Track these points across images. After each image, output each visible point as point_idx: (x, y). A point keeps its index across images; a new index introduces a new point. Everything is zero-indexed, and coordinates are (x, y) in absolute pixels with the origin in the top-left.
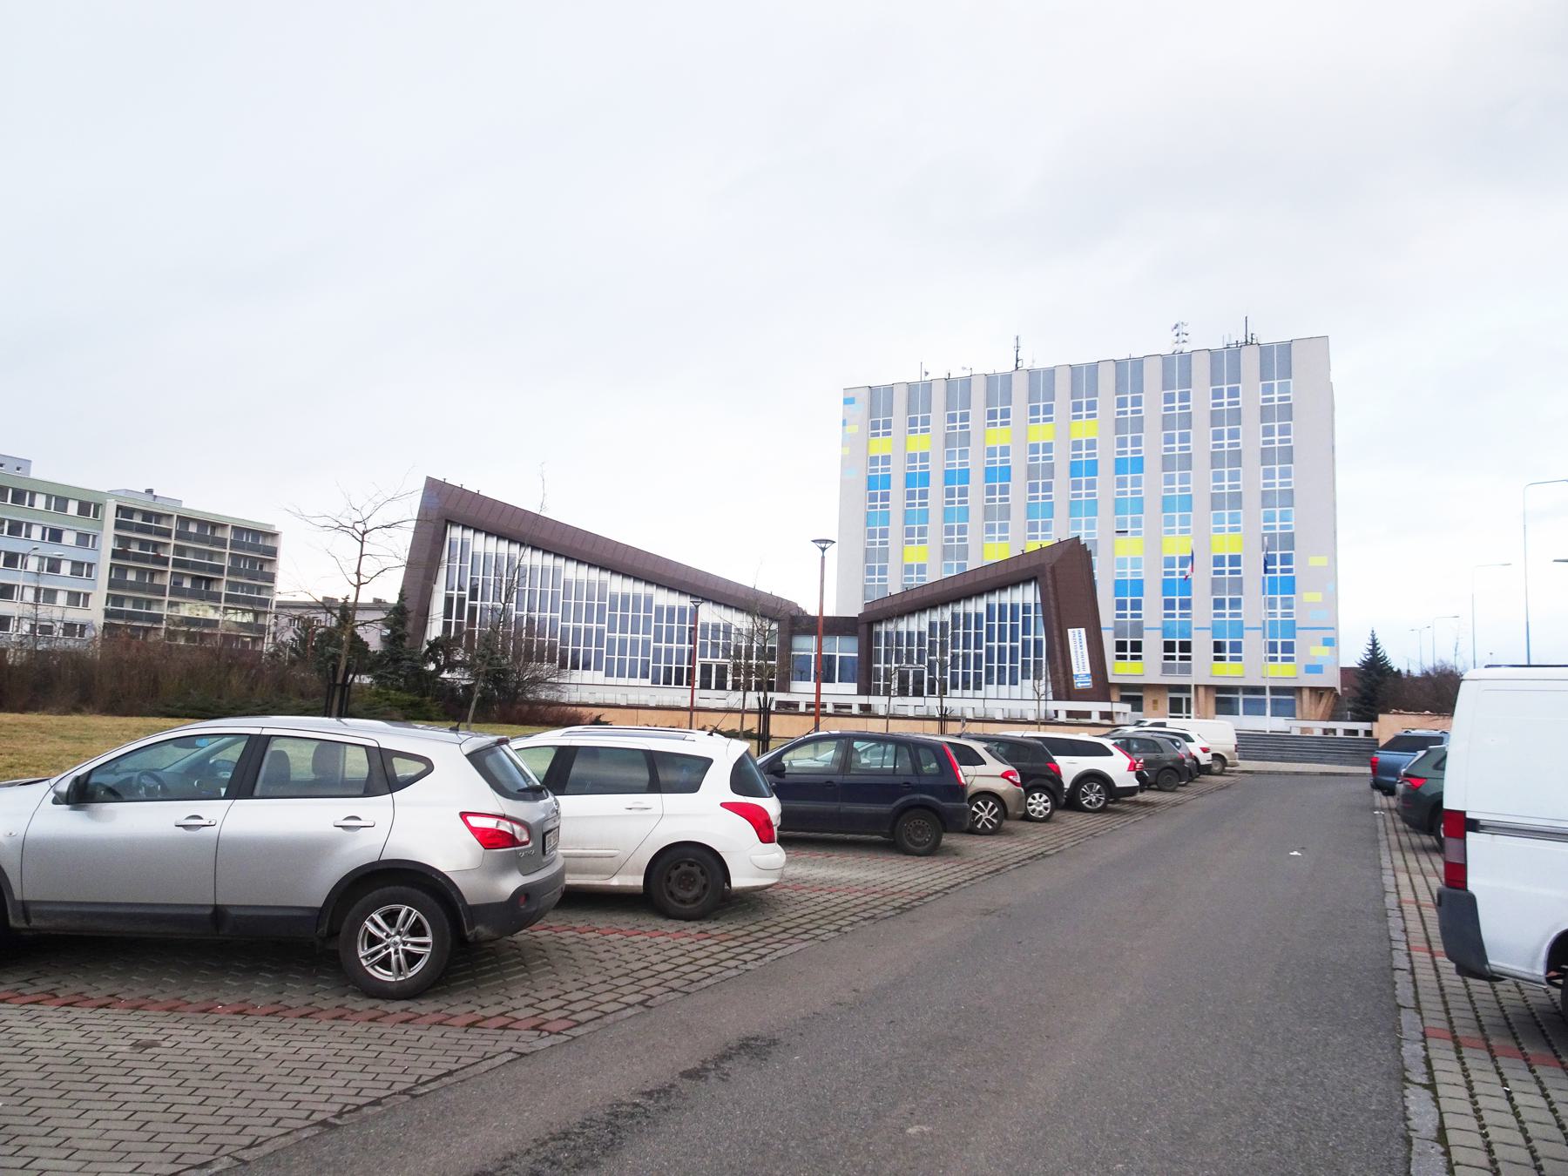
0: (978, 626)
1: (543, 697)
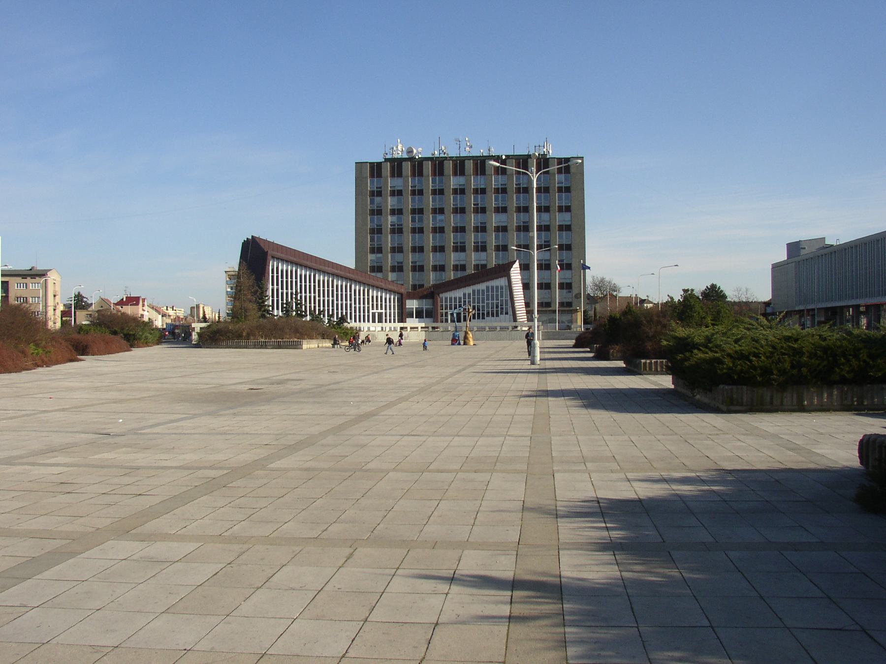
0: (483, 294)
1: (426, 293)
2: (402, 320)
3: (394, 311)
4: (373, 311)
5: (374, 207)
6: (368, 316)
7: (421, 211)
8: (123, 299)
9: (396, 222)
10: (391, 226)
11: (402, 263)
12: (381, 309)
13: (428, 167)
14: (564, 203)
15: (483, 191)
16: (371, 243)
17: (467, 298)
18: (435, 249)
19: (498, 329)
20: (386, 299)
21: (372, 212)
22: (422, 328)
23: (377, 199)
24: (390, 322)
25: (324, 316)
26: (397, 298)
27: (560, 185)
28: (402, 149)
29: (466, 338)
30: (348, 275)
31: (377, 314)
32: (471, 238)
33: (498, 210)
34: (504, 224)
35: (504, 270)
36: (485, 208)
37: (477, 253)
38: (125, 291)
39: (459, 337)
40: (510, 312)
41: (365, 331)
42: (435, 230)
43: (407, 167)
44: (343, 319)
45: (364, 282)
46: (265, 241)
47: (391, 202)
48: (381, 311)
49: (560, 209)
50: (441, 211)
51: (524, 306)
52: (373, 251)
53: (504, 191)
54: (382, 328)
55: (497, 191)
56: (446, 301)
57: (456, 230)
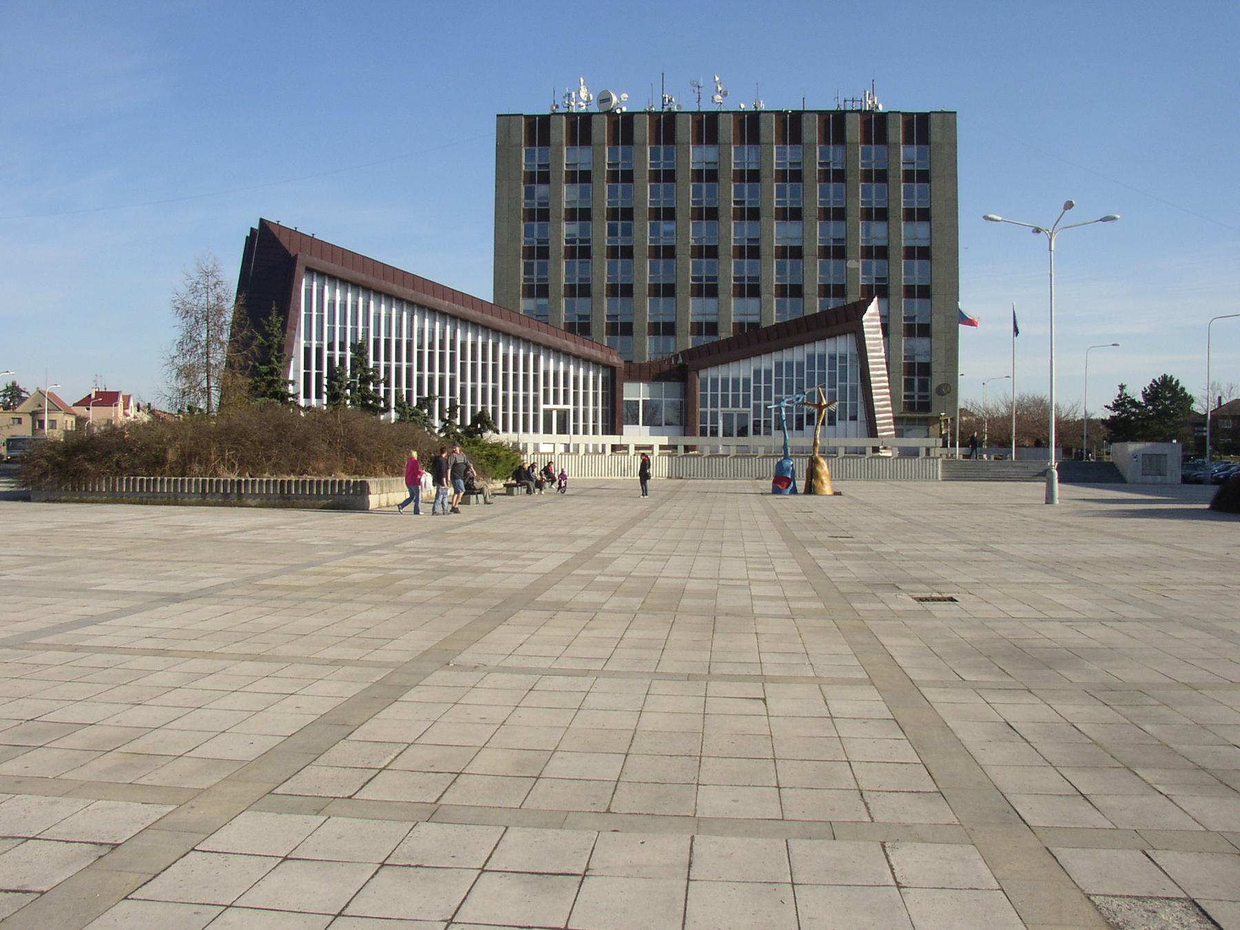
0: (800, 373)
2: (612, 427)
3: (595, 408)
4: (547, 407)
5: (534, 204)
6: (536, 418)
7: (628, 214)
8: (90, 395)
9: (578, 236)
10: (566, 243)
11: (587, 317)
12: (566, 402)
13: (643, 131)
14: (916, 203)
15: (755, 176)
16: (526, 276)
17: (741, 389)
18: (655, 291)
19: (841, 452)
20: (576, 379)
21: (530, 215)
22: (662, 447)
23: (540, 190)
24: (585, 432)
25: (431, 412)
26: (603, 377)
27: (909, 167)
28: (588, 97)
29: (812, 474)
30: (489, 317)
31: (555, 414)
32: (729, 270)
33: (782, 215)
34: (796, 244)
35: (848, 321)
36: (758, 209)
37: (741, 300)
38: (95, 381)
39: (793, 472)
40: (861, 414)
41: (557, 453)
42: (655, 252)
43: (601, 130)
44: (482, 421)
45: (527, 337)
46: (293, 233)
47: (567, 195)
48: (566, 407)
49: (909, 215)
50: (670, 214)
51: (889, 402)
52: (529, 292)
53: (797, 176)
54: (567, 447)
55: (782, 176)
56: (714, 388)
57: (698, 252)
